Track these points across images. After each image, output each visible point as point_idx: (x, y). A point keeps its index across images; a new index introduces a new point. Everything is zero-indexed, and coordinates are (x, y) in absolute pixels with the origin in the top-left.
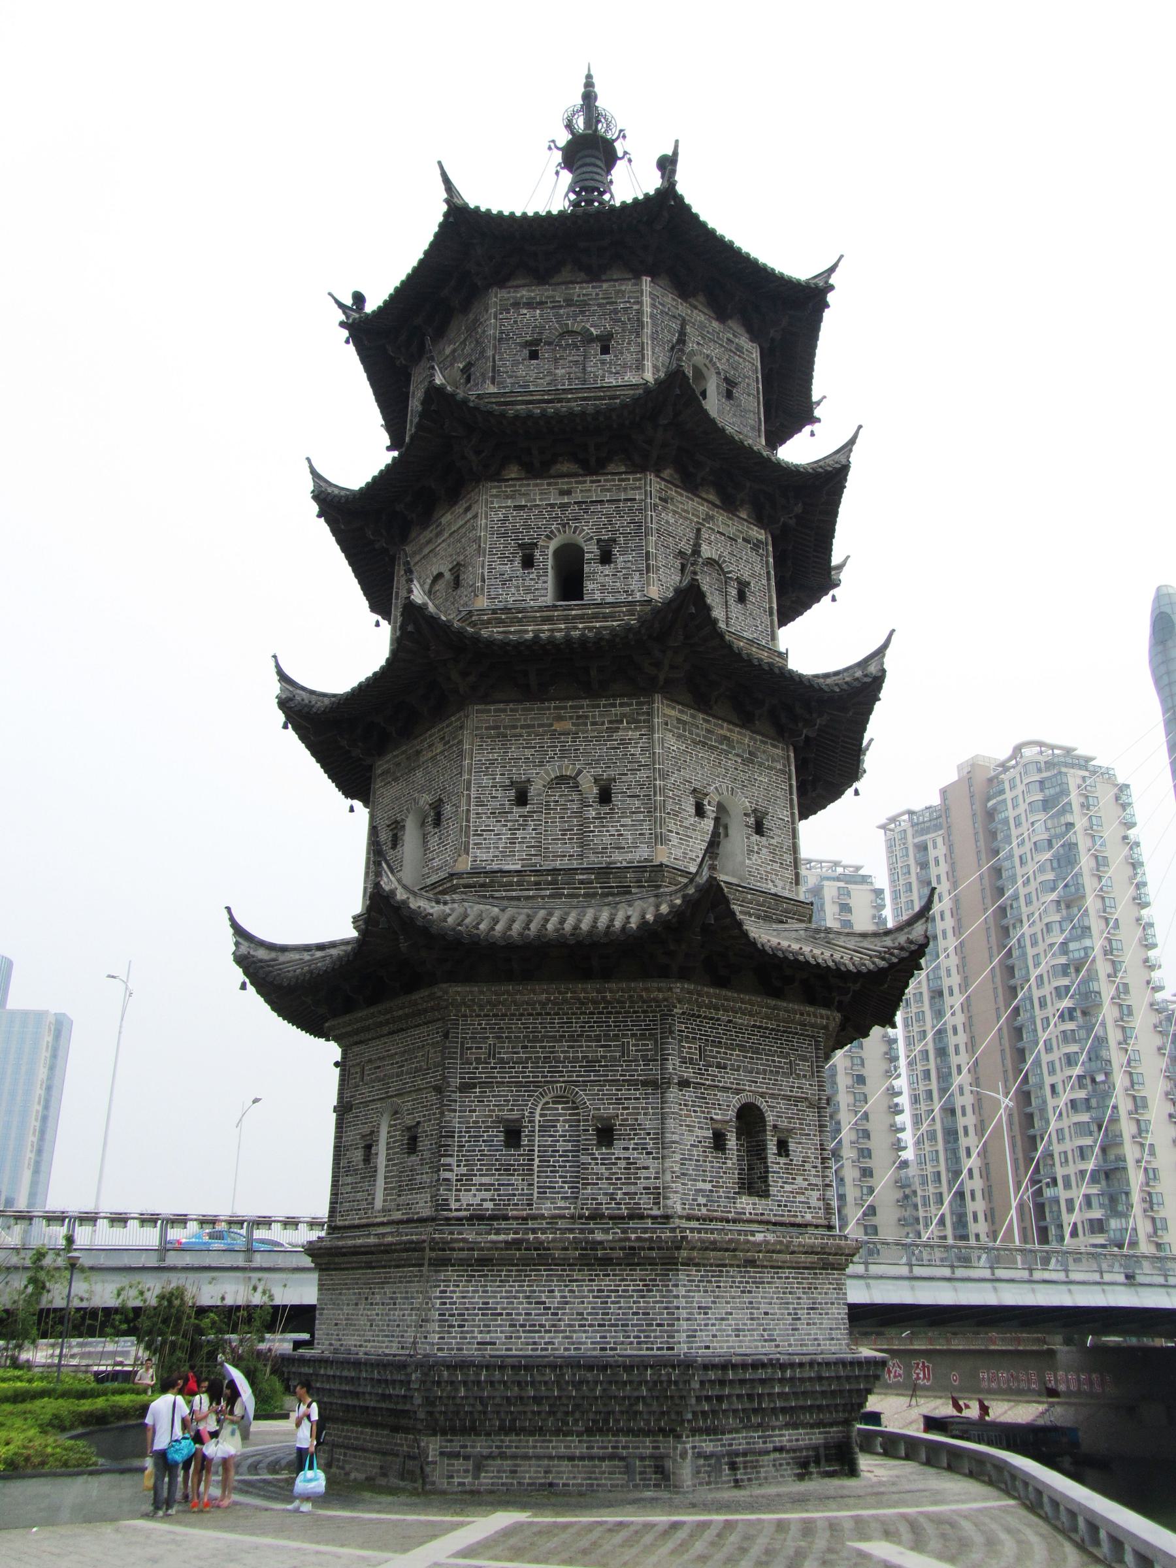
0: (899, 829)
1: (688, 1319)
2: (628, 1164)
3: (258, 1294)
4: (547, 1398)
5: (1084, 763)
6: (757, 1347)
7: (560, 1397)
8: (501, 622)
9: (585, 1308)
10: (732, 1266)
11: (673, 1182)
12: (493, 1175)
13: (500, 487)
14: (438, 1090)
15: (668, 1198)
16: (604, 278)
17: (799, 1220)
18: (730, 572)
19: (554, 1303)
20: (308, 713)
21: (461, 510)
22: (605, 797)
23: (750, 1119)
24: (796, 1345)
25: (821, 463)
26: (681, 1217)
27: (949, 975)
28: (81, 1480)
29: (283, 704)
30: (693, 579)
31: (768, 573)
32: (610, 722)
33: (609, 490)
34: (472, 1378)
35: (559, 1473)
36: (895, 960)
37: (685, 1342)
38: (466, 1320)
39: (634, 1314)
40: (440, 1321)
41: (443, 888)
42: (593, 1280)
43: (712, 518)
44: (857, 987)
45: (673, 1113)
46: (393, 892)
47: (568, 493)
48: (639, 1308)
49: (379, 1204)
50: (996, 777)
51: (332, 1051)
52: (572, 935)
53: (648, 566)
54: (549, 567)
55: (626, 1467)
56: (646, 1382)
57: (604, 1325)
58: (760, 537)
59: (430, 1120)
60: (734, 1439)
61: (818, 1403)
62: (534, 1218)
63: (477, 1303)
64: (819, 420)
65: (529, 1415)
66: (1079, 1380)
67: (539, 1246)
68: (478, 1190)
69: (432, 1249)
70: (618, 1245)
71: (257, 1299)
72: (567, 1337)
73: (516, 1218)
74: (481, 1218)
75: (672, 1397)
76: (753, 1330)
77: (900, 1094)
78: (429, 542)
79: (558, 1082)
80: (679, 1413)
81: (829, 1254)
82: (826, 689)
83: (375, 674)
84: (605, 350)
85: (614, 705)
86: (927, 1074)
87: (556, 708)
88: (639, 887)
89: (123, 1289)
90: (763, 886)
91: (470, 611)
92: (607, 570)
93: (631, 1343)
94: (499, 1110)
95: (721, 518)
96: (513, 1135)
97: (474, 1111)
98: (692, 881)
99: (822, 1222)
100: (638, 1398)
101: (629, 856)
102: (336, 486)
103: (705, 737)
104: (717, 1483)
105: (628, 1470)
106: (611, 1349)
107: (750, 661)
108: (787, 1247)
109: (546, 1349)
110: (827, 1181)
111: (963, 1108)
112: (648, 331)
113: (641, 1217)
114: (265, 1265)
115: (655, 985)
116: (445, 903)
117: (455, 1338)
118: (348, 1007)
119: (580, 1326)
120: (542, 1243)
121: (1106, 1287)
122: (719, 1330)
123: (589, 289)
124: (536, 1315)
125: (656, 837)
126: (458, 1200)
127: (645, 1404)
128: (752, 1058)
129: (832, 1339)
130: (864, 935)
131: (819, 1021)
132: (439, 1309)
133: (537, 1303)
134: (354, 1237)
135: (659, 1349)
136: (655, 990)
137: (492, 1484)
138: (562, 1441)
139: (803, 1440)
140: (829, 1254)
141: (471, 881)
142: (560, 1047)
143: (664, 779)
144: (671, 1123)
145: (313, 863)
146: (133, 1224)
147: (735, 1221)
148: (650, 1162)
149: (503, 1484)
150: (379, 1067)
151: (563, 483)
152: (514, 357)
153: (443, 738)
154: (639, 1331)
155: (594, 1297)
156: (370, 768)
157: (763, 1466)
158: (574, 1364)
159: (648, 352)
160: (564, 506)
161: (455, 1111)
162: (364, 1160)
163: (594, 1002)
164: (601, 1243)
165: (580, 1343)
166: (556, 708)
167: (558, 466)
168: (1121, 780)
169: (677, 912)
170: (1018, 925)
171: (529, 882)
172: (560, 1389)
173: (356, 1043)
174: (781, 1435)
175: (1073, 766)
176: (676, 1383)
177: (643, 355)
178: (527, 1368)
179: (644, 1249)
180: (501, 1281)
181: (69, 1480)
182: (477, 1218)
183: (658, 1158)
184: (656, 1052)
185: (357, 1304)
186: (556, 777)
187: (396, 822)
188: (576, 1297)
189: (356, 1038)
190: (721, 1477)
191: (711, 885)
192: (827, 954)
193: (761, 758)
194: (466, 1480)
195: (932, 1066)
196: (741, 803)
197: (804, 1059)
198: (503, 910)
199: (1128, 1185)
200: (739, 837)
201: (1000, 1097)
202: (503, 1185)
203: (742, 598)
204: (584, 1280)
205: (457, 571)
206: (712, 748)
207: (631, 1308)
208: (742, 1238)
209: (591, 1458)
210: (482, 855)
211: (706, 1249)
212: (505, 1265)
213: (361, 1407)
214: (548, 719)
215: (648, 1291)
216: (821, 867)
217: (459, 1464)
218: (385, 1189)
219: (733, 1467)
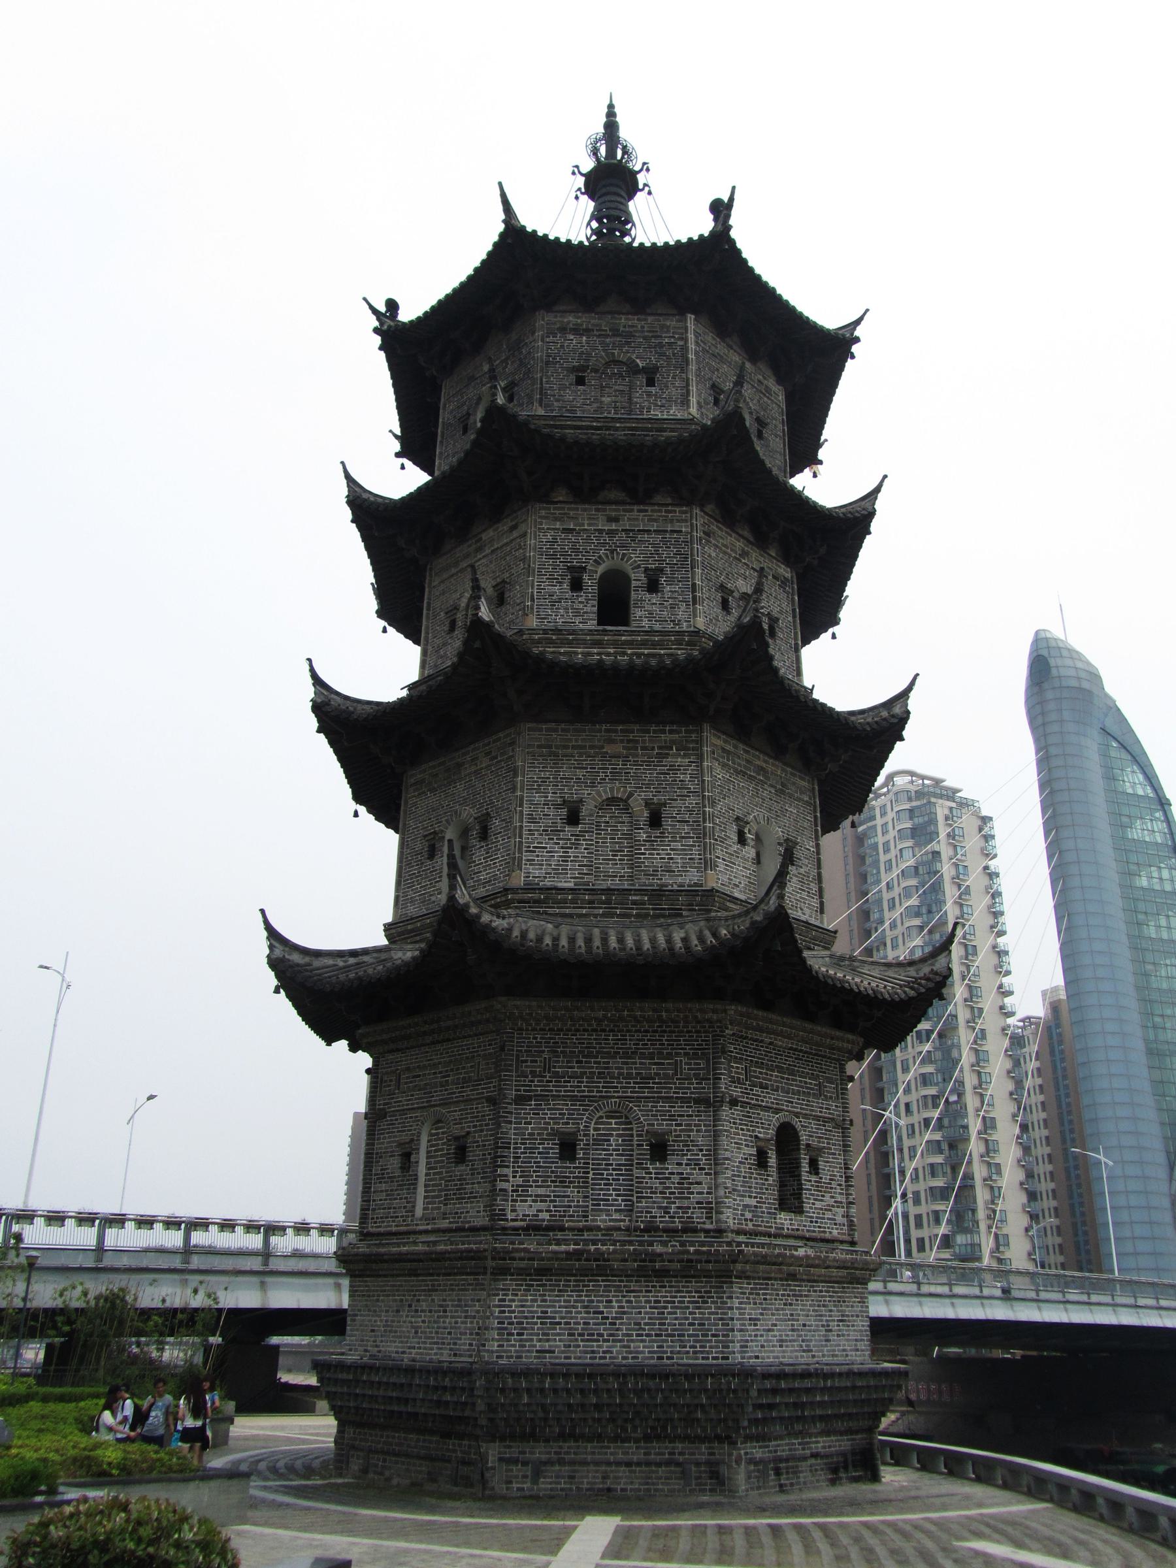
1: (741, 1330)
3: (201, 1295)
4: (609, 1405)
5: (950, 794)
6: (797, 1357)
7: (621, 1405)
8: (551, 642)
10: (776, 1279)
11: (727, 1197)
14: (492, 1101)
15: (722, 1213)
16: (649, 311)
17: (827, 1236)
22: (655, 820)
23: (786, 1137)
26: (732, 1231)
28: (192, 1485)
32: (660, 748)
33: (655, 520)
34: (537, 1385)
35: (616, 1478)
36: (923, 990)
38: (525, 1329)
39: (690, 1324)
40: (499, 1329)
42: (650, 1291)
47: (616, 520)
48: (694, 1319)
49: (419, 1212)
51: (364, 1060)
53: (694, 598)
55: (683, 1472)
56: (706, 1390)
57: (661, 1335)
59: (482, 1131)
60: (778, 1446)
61: (850, 1411)
62: (589, 1229)
63: (536, 1312)
64: (821, 462)
65: (590, 1422)
66: (929, 1390)
67: (599, 1256)
68: (534, 1201)
69: (493, 1259)
70: (676, 1258)
71: (198, 1301)
72: (624, 1347)
73: (571, 1229)
75: (729, 1405)
78: (467, 556)
79: (613, 1097)
80: (737, 1421)
81: (856, 1269)
84: (651, 383)
87: (607, 731)
89: (65, 1289)
92: (655, 598)
93: (688, 1352)
94: (555, 1123)
95: (754, 554)
96: (568, 1148)
97: (530, 1123)
99: (846, 1238)
100: (697, 1406)
101: (680, 880)
103: (745, 767)
105: (684, 1475)
106: (668, 1358)
107: (798, 697)
109: (605, 1358)
110: (851, 1199)
112: (693, 367)
113: (695, 1231)
114: (202, 1267)
115: (711, 1006)
116: (504, 918)
117: (514, 1346)
119: (638, 1335)
120: (603, 1254)
121: (985, 1301)
123: (634, 321)
124: (595, 1324)
125: (706, 863)
127: (704, 1411)
128: (788, 1079)
132: (498, 1318)
134: (398, 1245)
135: (713, 1358)
137: (551, 1489)
138: (619, 1447)
142: (614, 1063)
144: (724, 1141)
146: (158, 1226)
147: (776, 1236)
149: (562, 1490)
151: (612, 511)
152: (560, 377)
154: (695, 1341)
157: (802, 1472)
158: (638, 1372)
159: (693, 389)
160: (611, 533)
162: (401, 1168)
164: (661, 1255)
165: (638, 1352)
166: (607, 731)
168: (984, 813)
170: (882, 948)
171: (583, 901)
172: (622, 1396)
174: (817, 1442)
175: (941, 796)
176: (735, 1391)
177: (688, 392)
178: (591, 1376)
179: (700, 1262)
180: (559, 1291)
181: (182, 1485)
182: (534, 1228)
183: (710, 1174)
185: (398, 1311)
188: (634, 1308)
199: (975, 1202)
204: (641, 1291)
207: (687, 1319)
208: (788, 1252)
209: (648, 1464)
211: (758, 1263)
212: (563, 1275)
213: (408, 1413)
214: (599, 741)
215: (704, 1302)
217: (516, 1469)
218: (425, 1197)
219: (778, 1472)
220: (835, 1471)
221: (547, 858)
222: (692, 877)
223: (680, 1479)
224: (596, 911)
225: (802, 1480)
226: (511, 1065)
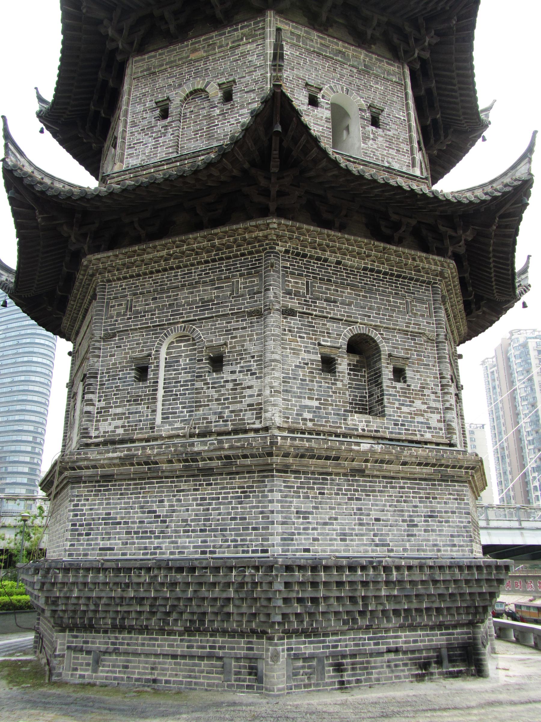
1: (283, 523)
2: (235, 385)
9: (190, 516)
10: (337, 474)
11: (272, 396)
12: (125, 406)
17: (418, 438)
19: (162, 511)
24: (411, 550)
35: (163, 669)
37: (280, 545)
42: (197, 490)
45: (273, 335)
57: (205, 530)
60: (339, 641)
63: (101, 514)
72: (172, 542)
73: (141, 440)
74: (113, 442)
76: (362, 535)
85: (237, 30)
93: (229, 546)
94: (132, 352)
96: (142, 372)
104: (317, 685)
105: (224, 670)
108: (397, 458)
110: (447, 405)
119: (185, 531)
122: (321, 534)
126: (97, 429)
129: (454, 545)
132: (72, 521)
133: (149, 512)
135: (254, 551)
138: (166, 640)
139: (422, 641)
140: (447, 466)
142: (182, 294)
148: (254, 382)
149: (115, 678)
154: (237, 535)
155: (197, 505)
164: (199, 453)
190: (323, 679)
193: (376, 70)
194: (86, 673)
197: (421, 301)
200: (357, 127)
202: (132, 413)
204: (189, 490)
207: (229, 514)
209: (192, 657)
211: (303, 456)
215: (246, 497)
217: (82, 658)
219: (339, 668)
220: (425, 665)
223: (222, 673)
225: (374, 676)
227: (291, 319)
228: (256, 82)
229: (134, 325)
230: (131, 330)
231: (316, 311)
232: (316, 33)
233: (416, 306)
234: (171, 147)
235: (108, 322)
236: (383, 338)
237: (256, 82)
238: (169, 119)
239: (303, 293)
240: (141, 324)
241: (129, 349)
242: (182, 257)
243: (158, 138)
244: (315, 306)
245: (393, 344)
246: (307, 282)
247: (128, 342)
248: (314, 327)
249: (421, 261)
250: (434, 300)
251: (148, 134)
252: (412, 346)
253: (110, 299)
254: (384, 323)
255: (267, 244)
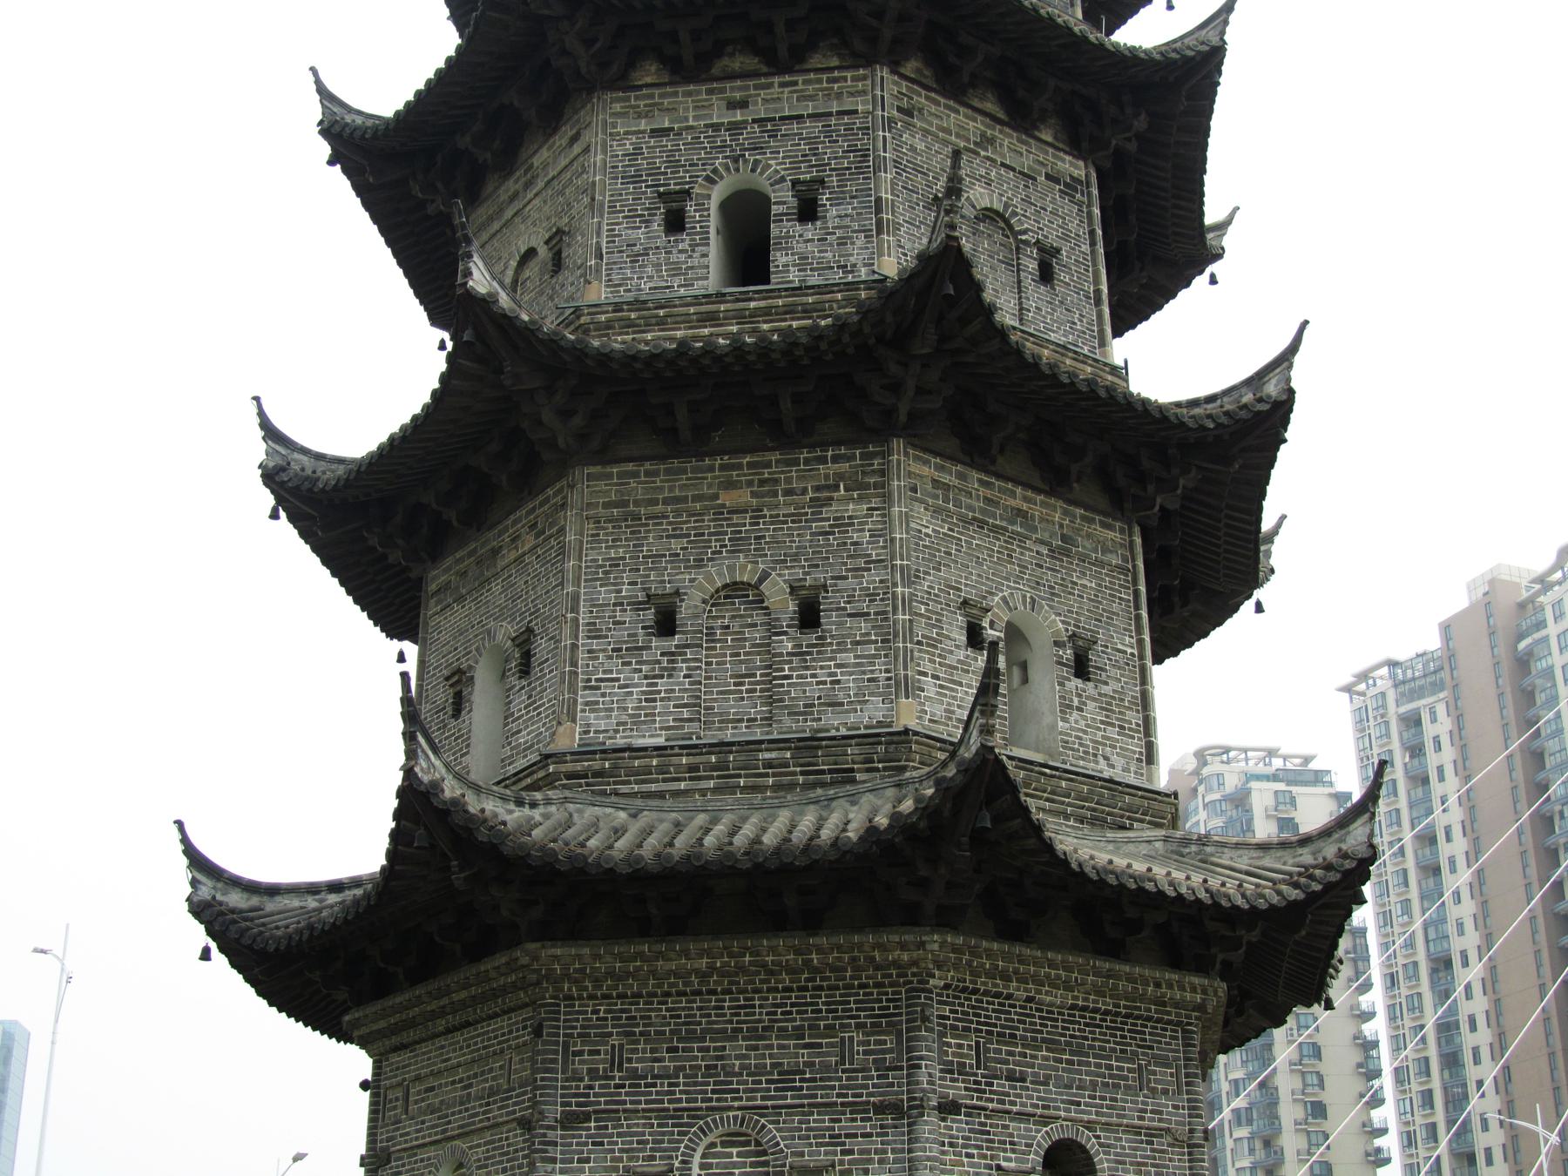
0: (1372, 692)
8: (629, 325)
13: (628, 100)
14: (526, 1124)
18: (1025, 232)
20: (310, 490)
21: (564, 142)
22: (809, 617)
25: (1178, 45)
27: (1461, 932)
29: (271, 477)
30: (948, 236)
31: (1092, 233)
32: (817, 489)
33: (811, 98)
36: (1317, 887)
41: (533, 779)
43: (991, 141)
44: (1254, 936)
45: (929, 1159)
46: (436, 786)
47: (743, 104)
50: (1531, 600)
51: (356, 1062)
52: (746, 853)
53: (879, 223)
54: (713, 231)
58: (1076, 173)
77: (1383, 1131)
78: (514, 197)
82: (1191, 424)
83: (415, 418)
85: (823, 460)
86: (1427, 1098)
88: (868, 770)
90: (1090, 767)
91: (577, 309)
92: (810, 231)
94: (630, 1159)
95: (1008, 143)
97: (587, 1160)
98: (953, 755)
101: (852, 718)
102: (360, 113)
103: (983, 511)
111: (1488, 1151)
116: (533, 805)
118: (382, 987)
125: (898, 684)
130: (1264, 847)
131: (1188, 995)
136: (896, 946)
141: (578, 767)
142: (734, 1048)
143: (910, 584)
145: (314, 741)
150: (432, 1089)
153: (534, 526)
156: (419, 583)
160: (735, 128)
161: (554, 1160)
163: (793, 971)
166: (723, 468)
167: (726, 61)
169: (926, 810)
173: (396, 1049)
184: (900, 1053)
186: (726, 586)
187: (459, 671)
189: (395, 1040)
191: (984, 761)
192: (1197, 879)
193: (1083, 545)
195: (1436, 1084)
196: (1049, 624)
198: (634, 816)
200: (1048, 679)
201: (1539, 1129)
203: (1046, 275)
205: (557, 240)
206: (995, 529)
210: (598, 722)
216: (1247, 759)
221: (620, 700)
222: (872, 712)
224: (704, 784)
226: (555, 1061)
227: (953, 1121)
228: (872, 597)
229: (632, 1102)
230: (625, 1111)
231: (992, 1100)
232: (976, 475)
233: (1154, 1073)
234: (685, 705)
235: (570, 1088)
236: (1101, 1145)
237: (872, 597)
238: (677, 639)
239: (971, 1066)
240: (647, 1102)
241: (622, 1151)
242: (737, 974)
243: (655, 677)
244: (991, 1092)
245: (1117, 1154)
246: (977, 1043)
247: (619, 1135)
248: (988, 1133)
249: (1170, 986)
250: (1186, 1059)
251: (629, 663)
252: (1147, 1157)
253: (571, 1035)
254: (1103, 1114)
255: (914, 975)
